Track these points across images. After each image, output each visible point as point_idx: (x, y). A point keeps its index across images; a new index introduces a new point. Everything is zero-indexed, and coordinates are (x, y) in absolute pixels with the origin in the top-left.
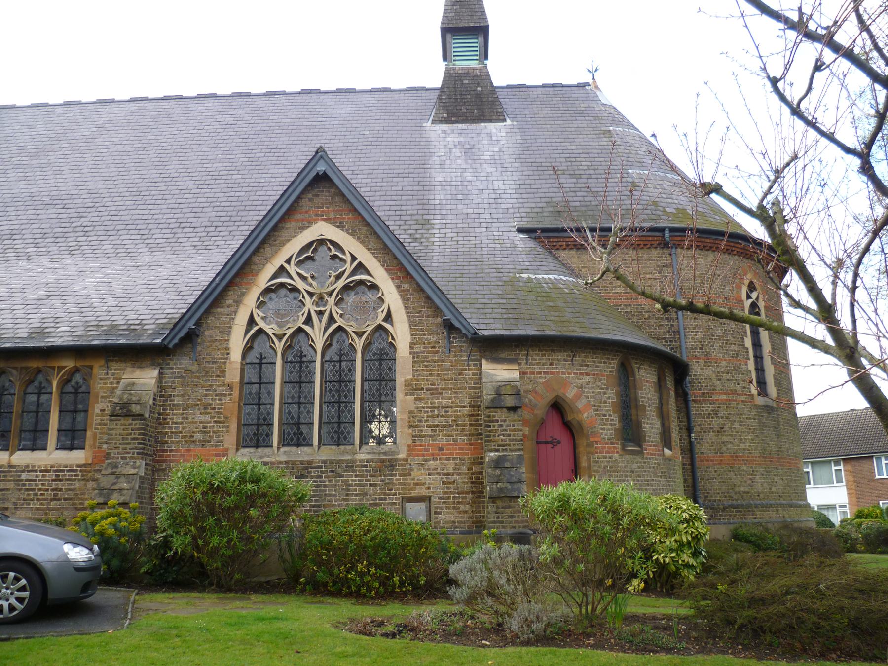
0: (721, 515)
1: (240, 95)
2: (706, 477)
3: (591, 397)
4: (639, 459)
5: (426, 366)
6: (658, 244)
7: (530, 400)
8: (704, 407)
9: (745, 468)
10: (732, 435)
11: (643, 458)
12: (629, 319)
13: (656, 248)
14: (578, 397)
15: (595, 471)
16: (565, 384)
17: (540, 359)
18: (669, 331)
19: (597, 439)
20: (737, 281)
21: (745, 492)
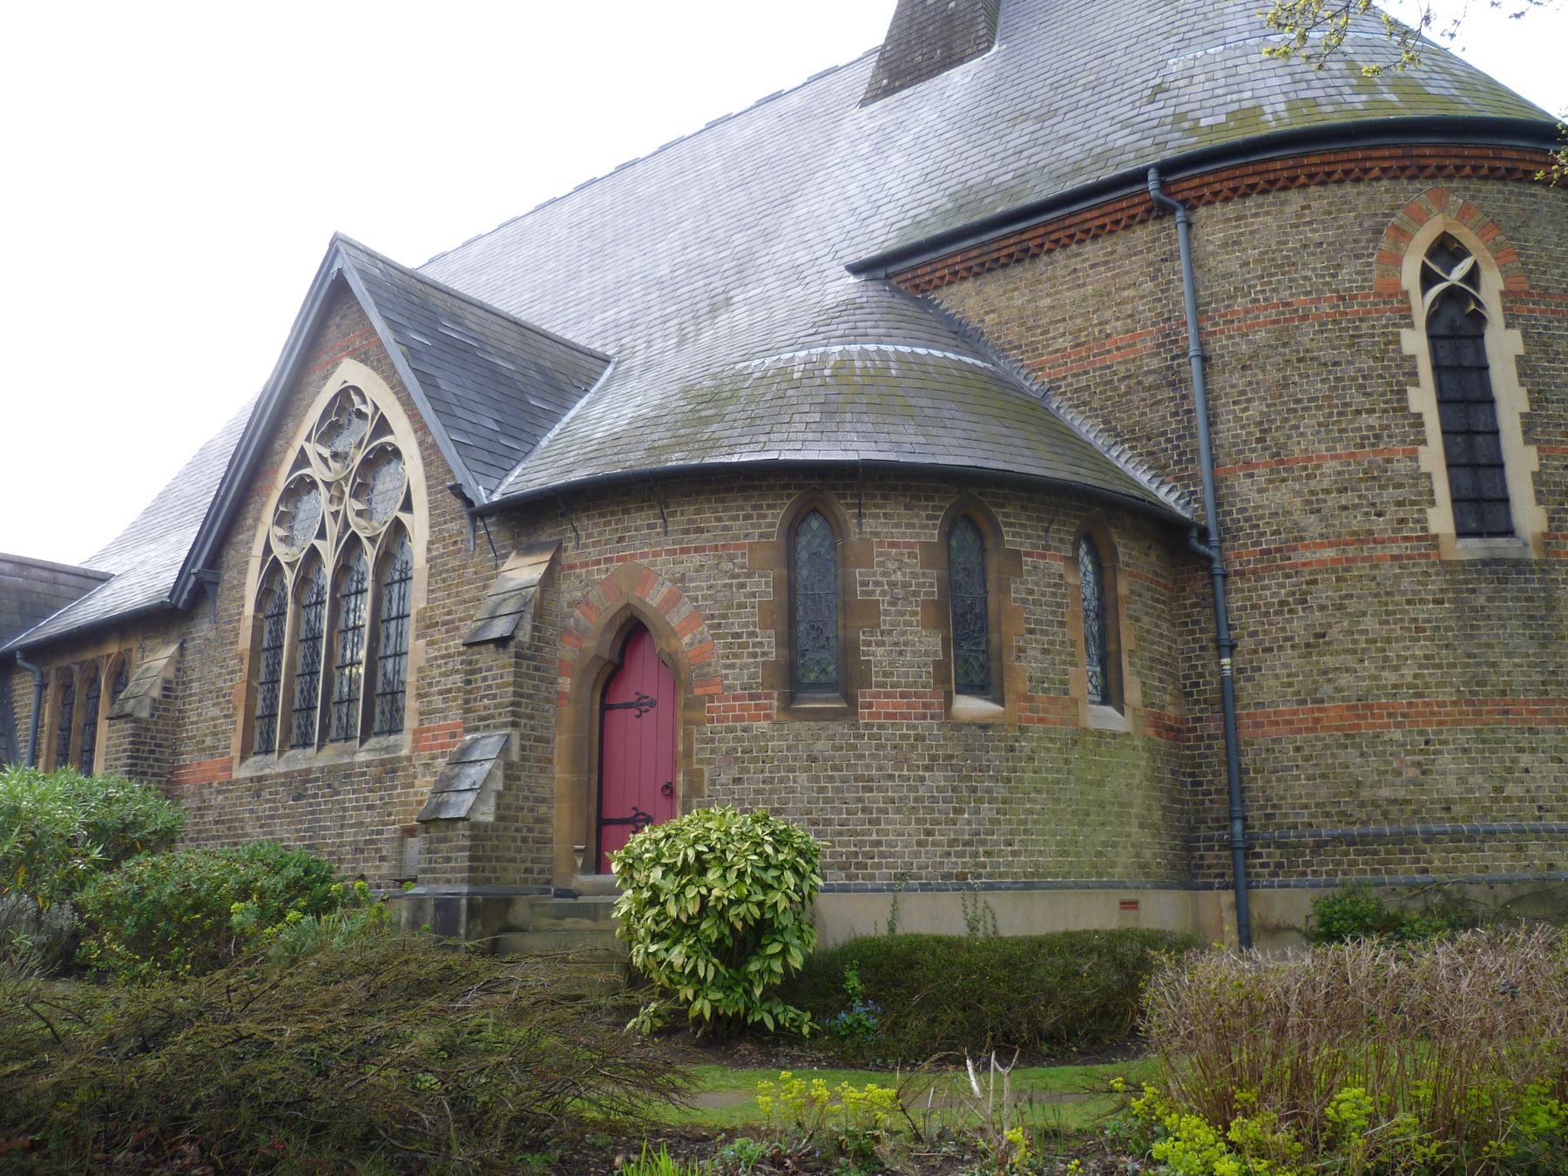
0: (1308, 864)
1: (623, 167)
2: (1270, 766)
3: (705, 598)
4: (838, 728)
5: (444, 580)
6: (1149, 211)
7: (577, 621)
9: (1397, 735)
10: (1354, 652)
11: (855, 726)
12: (1085, 404)
13: (1142, 222)
14: (672, 601)
15: (701, 761)
16: (645, 578)
17: (600, 534)
18: (1176, 414)
19: (711, 690)
20: (1385, 244)
21: (1395, 802)
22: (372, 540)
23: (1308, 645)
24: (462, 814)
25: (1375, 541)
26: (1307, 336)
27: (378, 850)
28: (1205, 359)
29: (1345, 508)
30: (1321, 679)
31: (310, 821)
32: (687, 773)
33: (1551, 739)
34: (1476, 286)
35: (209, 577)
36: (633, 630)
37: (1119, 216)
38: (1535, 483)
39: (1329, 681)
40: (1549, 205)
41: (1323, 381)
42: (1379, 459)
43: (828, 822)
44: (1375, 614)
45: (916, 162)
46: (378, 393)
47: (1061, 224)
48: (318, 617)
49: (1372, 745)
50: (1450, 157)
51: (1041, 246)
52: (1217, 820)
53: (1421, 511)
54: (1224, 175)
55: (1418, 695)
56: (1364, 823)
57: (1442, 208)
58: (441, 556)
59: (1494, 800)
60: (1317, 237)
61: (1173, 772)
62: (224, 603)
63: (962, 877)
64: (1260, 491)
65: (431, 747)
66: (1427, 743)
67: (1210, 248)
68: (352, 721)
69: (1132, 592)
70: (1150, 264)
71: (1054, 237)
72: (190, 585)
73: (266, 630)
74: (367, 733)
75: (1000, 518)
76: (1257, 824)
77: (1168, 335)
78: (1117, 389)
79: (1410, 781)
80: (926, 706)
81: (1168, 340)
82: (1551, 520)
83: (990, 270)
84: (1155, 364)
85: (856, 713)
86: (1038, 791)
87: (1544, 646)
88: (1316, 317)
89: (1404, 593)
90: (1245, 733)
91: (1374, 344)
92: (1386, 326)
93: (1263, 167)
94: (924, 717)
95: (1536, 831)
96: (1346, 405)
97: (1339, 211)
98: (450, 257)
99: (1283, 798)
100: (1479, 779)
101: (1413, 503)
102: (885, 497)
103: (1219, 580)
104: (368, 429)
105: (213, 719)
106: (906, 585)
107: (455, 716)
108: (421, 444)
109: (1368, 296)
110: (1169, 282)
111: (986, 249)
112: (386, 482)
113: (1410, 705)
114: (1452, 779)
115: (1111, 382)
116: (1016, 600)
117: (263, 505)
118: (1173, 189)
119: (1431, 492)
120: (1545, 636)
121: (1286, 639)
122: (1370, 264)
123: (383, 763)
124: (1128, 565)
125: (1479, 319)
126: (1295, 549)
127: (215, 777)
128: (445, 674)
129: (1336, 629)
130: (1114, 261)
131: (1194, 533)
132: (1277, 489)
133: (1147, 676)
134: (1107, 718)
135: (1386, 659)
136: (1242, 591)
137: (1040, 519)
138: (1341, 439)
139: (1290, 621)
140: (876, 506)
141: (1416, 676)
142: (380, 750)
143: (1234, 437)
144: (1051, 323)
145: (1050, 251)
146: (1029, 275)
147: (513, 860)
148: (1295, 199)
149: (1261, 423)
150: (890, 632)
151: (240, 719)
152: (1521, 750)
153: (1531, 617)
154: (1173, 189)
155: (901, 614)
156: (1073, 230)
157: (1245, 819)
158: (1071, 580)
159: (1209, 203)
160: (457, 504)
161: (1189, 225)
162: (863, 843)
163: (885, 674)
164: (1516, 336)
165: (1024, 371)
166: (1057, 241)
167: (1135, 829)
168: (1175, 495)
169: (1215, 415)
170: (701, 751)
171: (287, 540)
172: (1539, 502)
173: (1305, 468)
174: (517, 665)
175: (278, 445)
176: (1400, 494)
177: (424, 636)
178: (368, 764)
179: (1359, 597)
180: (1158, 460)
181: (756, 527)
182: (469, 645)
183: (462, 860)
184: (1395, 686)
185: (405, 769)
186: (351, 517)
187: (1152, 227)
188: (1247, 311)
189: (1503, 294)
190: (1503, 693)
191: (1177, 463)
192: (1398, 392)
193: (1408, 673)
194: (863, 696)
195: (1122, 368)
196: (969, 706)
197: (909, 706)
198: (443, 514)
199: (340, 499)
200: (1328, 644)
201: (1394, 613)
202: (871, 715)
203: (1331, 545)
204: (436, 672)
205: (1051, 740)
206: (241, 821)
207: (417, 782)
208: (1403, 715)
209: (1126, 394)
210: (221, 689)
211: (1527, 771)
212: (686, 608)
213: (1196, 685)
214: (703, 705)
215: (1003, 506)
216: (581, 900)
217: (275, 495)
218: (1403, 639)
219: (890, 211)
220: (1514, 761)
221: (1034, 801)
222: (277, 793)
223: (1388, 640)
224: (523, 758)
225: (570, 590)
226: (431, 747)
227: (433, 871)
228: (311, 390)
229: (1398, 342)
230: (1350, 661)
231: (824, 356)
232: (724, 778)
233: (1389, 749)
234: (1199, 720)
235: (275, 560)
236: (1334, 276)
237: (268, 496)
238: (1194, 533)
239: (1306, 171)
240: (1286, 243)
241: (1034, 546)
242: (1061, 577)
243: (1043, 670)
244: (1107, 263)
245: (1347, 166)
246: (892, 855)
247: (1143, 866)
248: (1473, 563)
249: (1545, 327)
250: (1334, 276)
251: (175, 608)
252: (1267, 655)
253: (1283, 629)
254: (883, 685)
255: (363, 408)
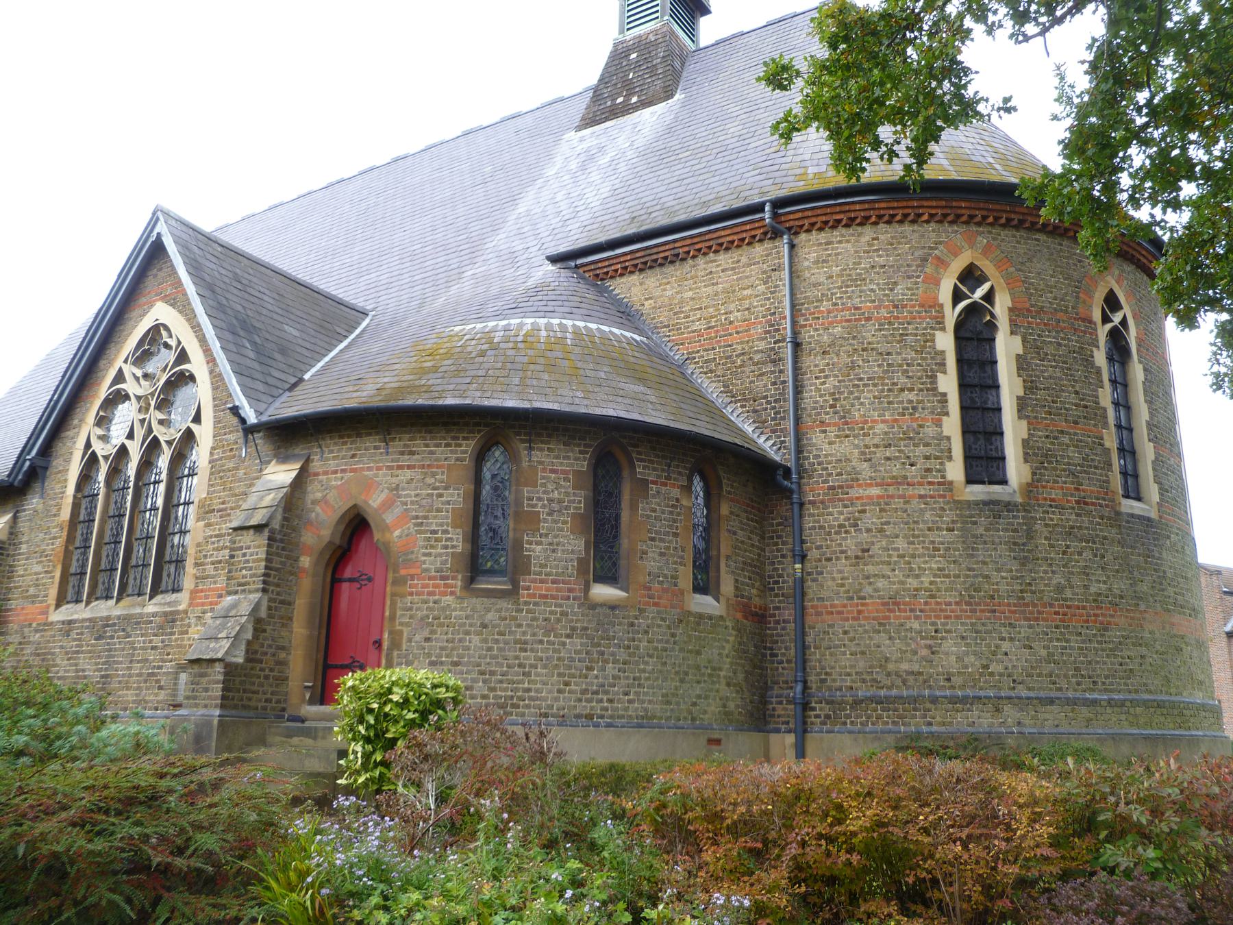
0: (848, 716)
1: (397, 160)
2: (825, 644)
3: (412, 503)
4: (503, 604)
5: (221, 478)
6: (765, 234)
7: (318, 515)
8: (831, 514)
9: (916, 625)
11: (517, 603)
12: (711, 371)
13: (760, 241)
15: (401, 624)
17: (339, 451)
18: (774, 383)
19: (412, 571)
20: (929, 269)
22: (169, 443)
23: (857, 557)
24: (220, 655)
25: (908, 484)
26: (870, 332)
27: (157, 681)
28: (797, 345)
29: (888, 459)
30: (864, 582)
31: (108, 657)
32: (391, 633)
33: (1025, 632)
34: (992, 304)
35: (40, 463)
36: (357, 526)
37: (744, 235)
38: (1024, 447)
39: (870, 584)
40: (1048, 248)
41: (879, 366)
42: (915, 425)
43: (492, 673)
44: (906, 537)
45: (604, 180)
46: (180, 330)
47: (703, 238)
48: (124, 498)
49: (898, 632)
50: (979, 209)
51: (688, 252)
52: (787, 682)
53: (941, 464)
54: (819, 212)
55: (932, 596)
56: (890, 688)
57: (972, 245)
58: (221, 459)
59: (981, 674)
60: (881, 261)
61: (755, 646)
62: (51, 484)
63: (590, 717)
64: (830, 443)
65: (203, 604)
66: (936, 631)
67: (806, 264)
68: (144, 582)
69: (732, 513)
70: (763, 272)
71: (697, 247)
72: (25, 468)
73: (83, 507)
74: (155, 591)
75: (634, 455)
76: (814, 686)
77: (773, 325)
78: (734, 362)
79: (923, 658)
80: (570, 590)
81: (772, 328)
82: (1034, 474)
83: (651, 267)
84: (762, 345)
85: (518, 593)
86: (651, 656)
87: (1023, 564)
88: (877, 319)
89: (925, 522)
90: (809, 620)
91: (916, 341)
92: (925, 329)
93: (847, 208)
94: (568, 598)
95: (1009, 698)
96: (894, 384)
97: (899, 243)
98: (258, 218)
99: (832, 668)
100: (972, 658)
101: (937, 458)
102: (549, 436)
103: (796, 507)
104: (172, 357)
105: (36, 574)
106: (560, 501)
107: (222, 582)
108: (211, 372)
109: (913, 306)
110: (776, 286)
111: (648, 252)
112: (183, 395)
113: (926, 603)
114: (953, 658)
115: (730, 357)
116: (642, 516)
117: (88, 410)
118: (783, 219)
119: (950, 450)
120: (1025, 558)
121: (842, 552)
122: (917, 283)
123: (165, 614)
124: (730, 493)
125: (992, 326)
126: (852, 487)
127: (34, 620)
128: (217, 549)
129: (877, 546)
130: (739, 268)
131: (780, 472)
132: (841, 442)
133: (739, 575)
134: (705, 604)
135: (911, 569)
136: (813, 515)
137: (664, 457)
138: (889, 409)
139: (845, 539)
140: (542, 442)
141: (931, 583)
142: (164, 604)
143: (815, 402)
144: (691, 310)
145: (694, 257)
146: (678, 273)
147: (256, 692)
148: (868, 233)
149: (834, 394)
150: (546, 535)
151: (58, 574)
152: (1003, 639)
153: (1015, 544)
154: (783, 219)
155: (556, 522)
156: (711, 243)
157: (805, 682)
158: (685, 502)
159: (808, 231)
160: (235, 420)
161: (792, 246)
162: (517, 689)
163: (541, 566)
164: (1018, 340)
165: (670, 344)
166: (699, 250)
167: (722, 686)
168: (770, 443)
169: (802, 386)
170: (402, 616)
171: (105, 438)
172: (1026, 461)
173: (863, 429)
174: (269, 546)
175: (102, 363)
176: (928, 451)
177: (204, 519)
178: (154, 615)
179: (895, 524)
180: (760, 416)
181: (450, 456)
182: (235, 529)
183: (217, 691)
184: (916, 590)
185: (182, 619)
186: (155, 425)
187: (768, 245)
188: (829, 312)
189: (1010, 310)
190: (992, 597)
191: (774, 419)
192: (931, 377)
193: (926, 579)
194: (524, 581)
195: (739, 347)
196: (603, 592)
197: (558, 590)
198: (224, 427)
199: (147, 409)
200: (871, 557)
201: (918, 536)
202: (529, 596)
203: (877, 485)
204: (210, 547)
205: (663, 620)
206: (53, 654)
207: (190, 630)
208: (921, 611)
209: (741, 366)
210: (44, 551)
211: (1006, 654)
212: (398, 510)
213: (777, 582)
214: (405, 583)
215: (637, 446)
216: (307, 724)
217: (97, 403)
218: (924, 555)
219: (585, 216)
220: (997, 647)
221: (647, 663)
222: (82, 634)
223: (913, 556)
224: (270, 616)
225: (314, 491)
226: (203, 604)
227: (195, 698)
228: (131, 323)
229: (933, 341)
230: (886, 570)
231: (521, 325)
232: (417, 637)
233: (909, 635)
234: (778, 608)
235: (94, 453)
236: (892, 290)
237: (92, 403)
238: (780, 472)
239: (877, 213)
240: (860, 263)
241: (659, 477)
242: (677, 500)
243: (660, 568)
244: (733, 269)
245: (906, 211)
246: (537, 699)
247: (726, 714)
248: (977, 503)
249: (1039, 335)
250: (892, 290)
251: (11, 485)
252: (829, 564)
253: (840, 545)
254: (540, 574)
255: (169, 341)
